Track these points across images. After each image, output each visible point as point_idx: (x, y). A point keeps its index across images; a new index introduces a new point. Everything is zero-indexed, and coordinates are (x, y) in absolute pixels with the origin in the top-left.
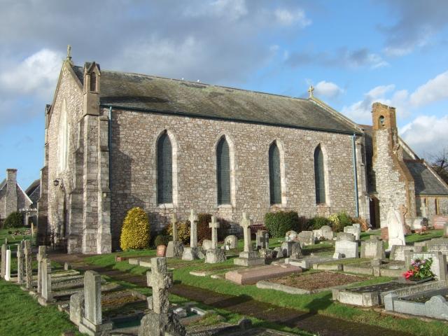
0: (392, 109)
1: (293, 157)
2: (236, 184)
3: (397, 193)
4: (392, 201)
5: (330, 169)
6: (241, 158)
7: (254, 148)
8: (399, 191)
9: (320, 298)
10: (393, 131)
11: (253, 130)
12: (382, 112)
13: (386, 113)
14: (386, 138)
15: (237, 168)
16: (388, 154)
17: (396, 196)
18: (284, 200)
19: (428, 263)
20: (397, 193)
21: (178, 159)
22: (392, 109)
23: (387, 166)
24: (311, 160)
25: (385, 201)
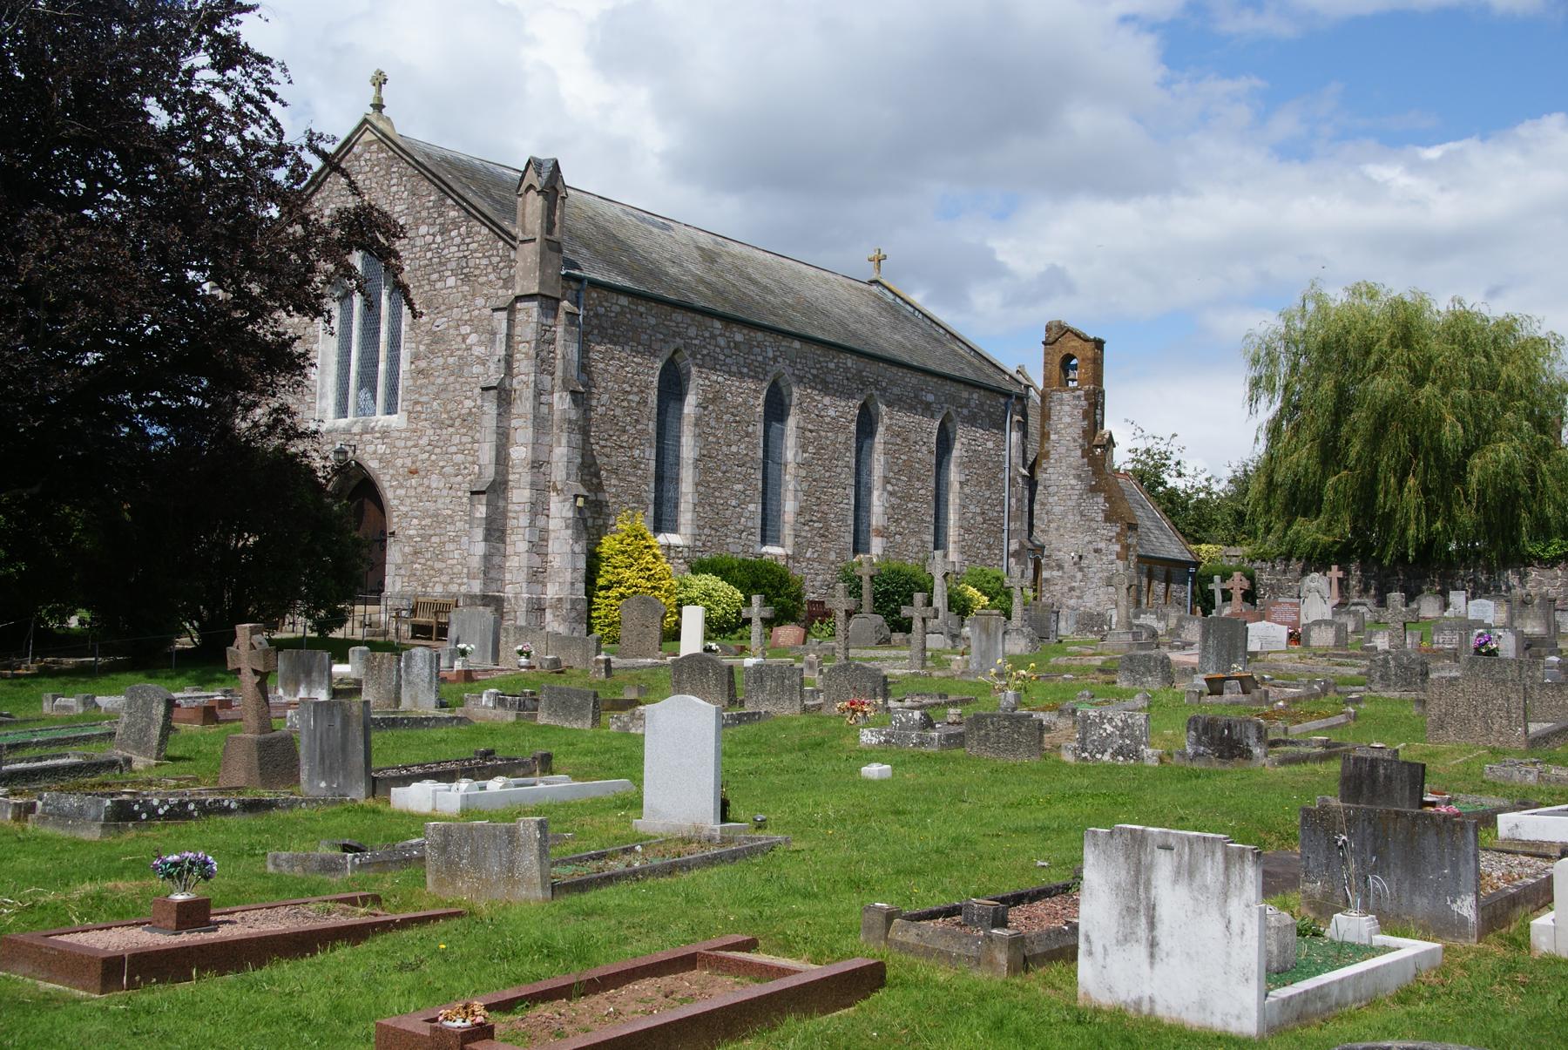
0: (1099, 344)
1: (899, 441)
2: (796, 497)
3: (1096, 551)
4: (1081, 569)
5: (963, 478)
6: (808, 434)
7: (832, 412)
8: (1102, 545)
9: (791, 1019)
10: (1095, 404)
11: (832, 366)
12: (1072, 345)
13: (1083, 351)
14: (1078, 413)
15: (799, 460)
16: (1079, 453)
17: (1092, 555)
18: (877, 545)
19: (675, 530)
20: (1096, 551)
21: (696, 425)
22: (1099, 344)
23: (1073, 482)
24: (930, 452)
25: (1060, 567)
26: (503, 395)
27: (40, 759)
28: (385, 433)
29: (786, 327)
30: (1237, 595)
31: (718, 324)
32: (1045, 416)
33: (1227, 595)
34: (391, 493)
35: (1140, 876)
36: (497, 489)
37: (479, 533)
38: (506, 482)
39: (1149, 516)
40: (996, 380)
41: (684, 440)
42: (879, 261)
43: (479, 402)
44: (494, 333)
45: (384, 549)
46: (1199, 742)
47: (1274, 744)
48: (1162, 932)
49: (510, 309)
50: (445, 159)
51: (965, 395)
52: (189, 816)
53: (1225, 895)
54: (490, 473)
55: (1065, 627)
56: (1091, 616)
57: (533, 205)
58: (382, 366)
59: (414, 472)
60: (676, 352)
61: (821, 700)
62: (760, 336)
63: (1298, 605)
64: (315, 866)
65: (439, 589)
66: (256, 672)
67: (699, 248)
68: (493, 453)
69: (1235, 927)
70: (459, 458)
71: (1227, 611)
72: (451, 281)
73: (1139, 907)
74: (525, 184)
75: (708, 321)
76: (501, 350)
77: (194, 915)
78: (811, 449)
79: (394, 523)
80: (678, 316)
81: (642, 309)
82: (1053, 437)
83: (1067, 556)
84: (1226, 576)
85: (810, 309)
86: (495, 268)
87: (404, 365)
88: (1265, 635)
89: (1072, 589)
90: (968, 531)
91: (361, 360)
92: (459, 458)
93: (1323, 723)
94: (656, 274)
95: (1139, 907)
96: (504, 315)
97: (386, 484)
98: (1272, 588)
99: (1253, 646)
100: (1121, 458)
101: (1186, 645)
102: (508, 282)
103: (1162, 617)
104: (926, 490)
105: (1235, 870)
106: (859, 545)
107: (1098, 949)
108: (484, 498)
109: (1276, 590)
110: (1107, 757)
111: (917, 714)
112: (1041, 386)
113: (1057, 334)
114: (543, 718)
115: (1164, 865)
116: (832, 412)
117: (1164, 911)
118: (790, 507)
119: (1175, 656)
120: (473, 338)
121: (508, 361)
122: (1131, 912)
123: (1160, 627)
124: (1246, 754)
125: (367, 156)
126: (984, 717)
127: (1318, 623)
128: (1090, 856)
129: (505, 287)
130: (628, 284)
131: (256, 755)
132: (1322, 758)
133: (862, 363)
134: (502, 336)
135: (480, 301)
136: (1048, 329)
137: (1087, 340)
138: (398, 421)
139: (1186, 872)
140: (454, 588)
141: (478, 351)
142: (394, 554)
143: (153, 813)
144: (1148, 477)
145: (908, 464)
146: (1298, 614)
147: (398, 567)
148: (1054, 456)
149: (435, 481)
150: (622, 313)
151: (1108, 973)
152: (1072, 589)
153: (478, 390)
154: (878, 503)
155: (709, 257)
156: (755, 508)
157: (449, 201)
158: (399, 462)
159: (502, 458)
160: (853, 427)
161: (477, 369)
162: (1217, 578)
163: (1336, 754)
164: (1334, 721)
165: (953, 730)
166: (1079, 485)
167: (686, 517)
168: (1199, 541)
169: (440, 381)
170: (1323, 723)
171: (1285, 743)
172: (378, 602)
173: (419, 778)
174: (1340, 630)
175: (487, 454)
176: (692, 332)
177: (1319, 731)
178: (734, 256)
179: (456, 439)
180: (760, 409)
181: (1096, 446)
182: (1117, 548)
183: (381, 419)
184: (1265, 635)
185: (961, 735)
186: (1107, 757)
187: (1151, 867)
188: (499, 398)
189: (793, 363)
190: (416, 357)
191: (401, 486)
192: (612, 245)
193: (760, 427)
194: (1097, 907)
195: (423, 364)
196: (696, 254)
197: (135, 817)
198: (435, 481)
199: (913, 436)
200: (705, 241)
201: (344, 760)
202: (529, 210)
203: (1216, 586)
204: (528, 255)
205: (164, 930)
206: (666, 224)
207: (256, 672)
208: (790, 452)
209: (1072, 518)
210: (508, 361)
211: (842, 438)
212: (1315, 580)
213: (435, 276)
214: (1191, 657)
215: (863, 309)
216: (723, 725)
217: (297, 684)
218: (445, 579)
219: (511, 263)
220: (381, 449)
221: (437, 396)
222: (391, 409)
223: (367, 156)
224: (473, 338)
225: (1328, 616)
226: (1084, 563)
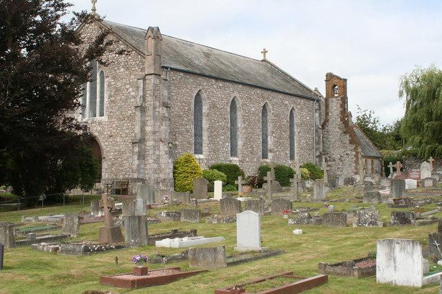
8: (349, 152)
10: (344, 101)
12: (336, 81)
14: (339, 106)
18: (270, 155)
19: (201, 153)
22: (346, 80)
26: (142, 109)
27: (43, 235)
28: (100, 123)
29: (236, 80)
30: (399, 169)
31: (213, 80)
32: (327, 107)
33: (395, 170)
34: (104, 144)
35: (392, 250)
36: (141, 141)
37: (136, 157)
38: (144, 139)
39: (365, 140)
40: (309, 95)
41: (203, 122)
42: (265, 52)
43: (134, 111)
44: (138, 88)
45: (101, 163)
46: (395, 219)
47: (417, 219)
48: (397, 264)
49: (144, 79)
50: (117, 27)
51: (299, 101)
52: (102, 250)
53: (412, 254)
54: (139, 136)
55: (341, 182)
56: (349, 178)
57: (151, 42)
58: (98, 100)
59: (111, 136)
60: (200, 91)
61: (270, 210)
62: (228, 84)
63: (420, 172)
64: (153, 261)
65: (121, 177)
66: (109, 208)
67: (204, 53)
68: (140, 130)
69: (416, 262)
70: (127, 131)
71: (395, 175)
72: (122, 70)
73: (391, 257)
74: (148, 35)
75: (210, 80)
76: (141, 93)
77: (144, 271)
78: (247, 123)
79: (104, 154)
80: (200, 79)
81: (188, 77)
82: (330, 114)
83: (337, 156)
84: (394, 163)
85: (243, 73)
86: (138, 65)
87: (106, 99)
88: (410, 183)
89: (338, 168)
90: (301, 149)
91: (90, 97)
92: (127, 131)
93: (431, 212)
94: (190, 64)
95: (391, 257)
96: (141, 81)
97: (103, 144)
98: (409, 165)
99: (407, 187)
100: (354, 120)
101: (383, 188)
102: (143, 70)
103: (373, 178)
104: (286, 135)
105: (415, 247)
106: (265, 156)
107: (381, 269)
108: (137, 145)
109: (411, 166)
110: (367, 225)
111: (306, 214)
112: (325, 96)
113: (330, 78)
114: (182, 219)
115: (397, 247)
116: (253, 109)
117: (398, 259)
118: (240, 143)
119: (381, 192)
120: (130, 90)
121: (144, 97)
122: (390, 259)
123: (373, 181)
124: (409, 222)
125: (91, 27)
126: (328, 214)
127: (427, 179)
128: (378, 246)
129: (141, 71)
130: (183, 68)
131: (110, 233)
132: (431, 223)
133: (263, 92)
134: (141, 89)
135: (133, 77)
136: (327, 76)
137: (341, 79)
138: (105, 118)
139: (402, 249)
140: (127, 176)
141: (133, 94)
142: (105, 165)
143: (94, 250)
144: (363, 126)
145: (280, 127)
146: (420, 175)
147: (107, 169)
148: (330, 121)
149: (119, 139)
150: (181, 79)
151: (385, 274)
152: (338, 168)
153: (133, 107)
154: (270, 141)
155: (207, 55)
156: (228, 144)
157: (121, 42)
158: (105, 133)
159: (143, 131)
160: (261, 114)
161: (133, 100)
162: (391, 163)
163: (436, 221)
164: (434, 211)
165: (317, 218)
166: (340, 131)
167: (205, 148)
168: (381, 148)
169: (119, 104)
170: (431, 212)
171: (420, 219)
172: (100, 182)
173: (164, 238)
174: (434, 180)
175: (137, 129)
176: (205, 83)
177: (430, 214)
178: (215, 54)
179: (126, 125)
180: (229, 110)
181: (345, 114)
182: (354, 153)
183: (98, 118)
184: (410, 183)
185: (321, 220)
186: (367, 225)
187: (394, 248)
188: (141, 110)
189: (239, 92)
190: (110, 96)
191: (106, 141)
192: (177, 55)
193: (229, 116)
194: (381, 260)
195: (113, 99)
196: (203, 55)
197: (89, 251)
198: (119, 139)
199: (282, 116)
200: (205, 50)
201: (140, 233)
202: (149, 44)
203: (391, 166)
204: (149, 60)
205: (138, 275)
206: (191, 45)
207: (109, 208)
208: (240, 124)
209: (338, 143)
210: (144, 97)
211: (257, 118)
212: (425, 164)
213: (116, 68)
214: (387, 192)
215: (261, 71)
216: (261, 219)
217: (98, 211)
218: (124, 173)
219: (143, 63)
220: (99, 129)
221: (118, 110)
222: (102, 115)
223: (91, 27)
224: (130, 90)
225: (430, 176)
226: (343, 159)
